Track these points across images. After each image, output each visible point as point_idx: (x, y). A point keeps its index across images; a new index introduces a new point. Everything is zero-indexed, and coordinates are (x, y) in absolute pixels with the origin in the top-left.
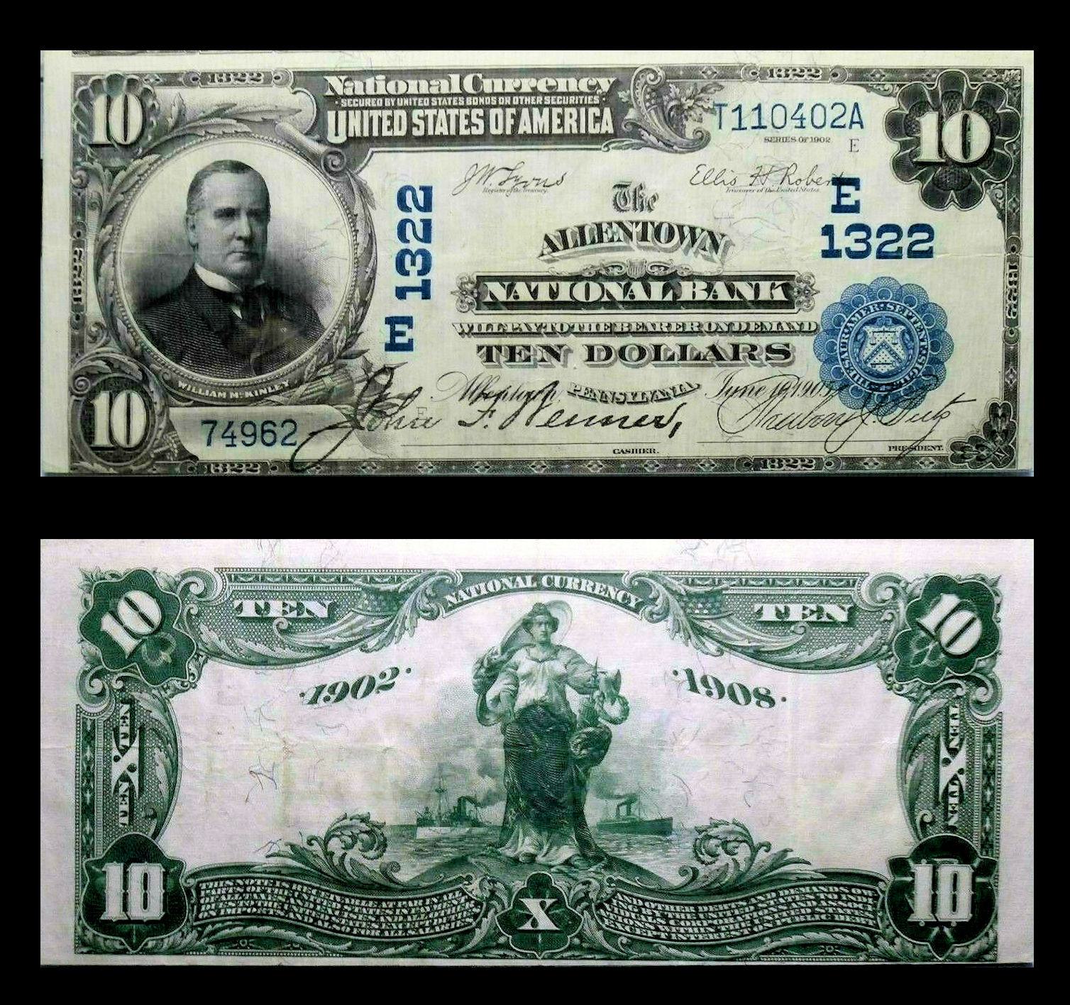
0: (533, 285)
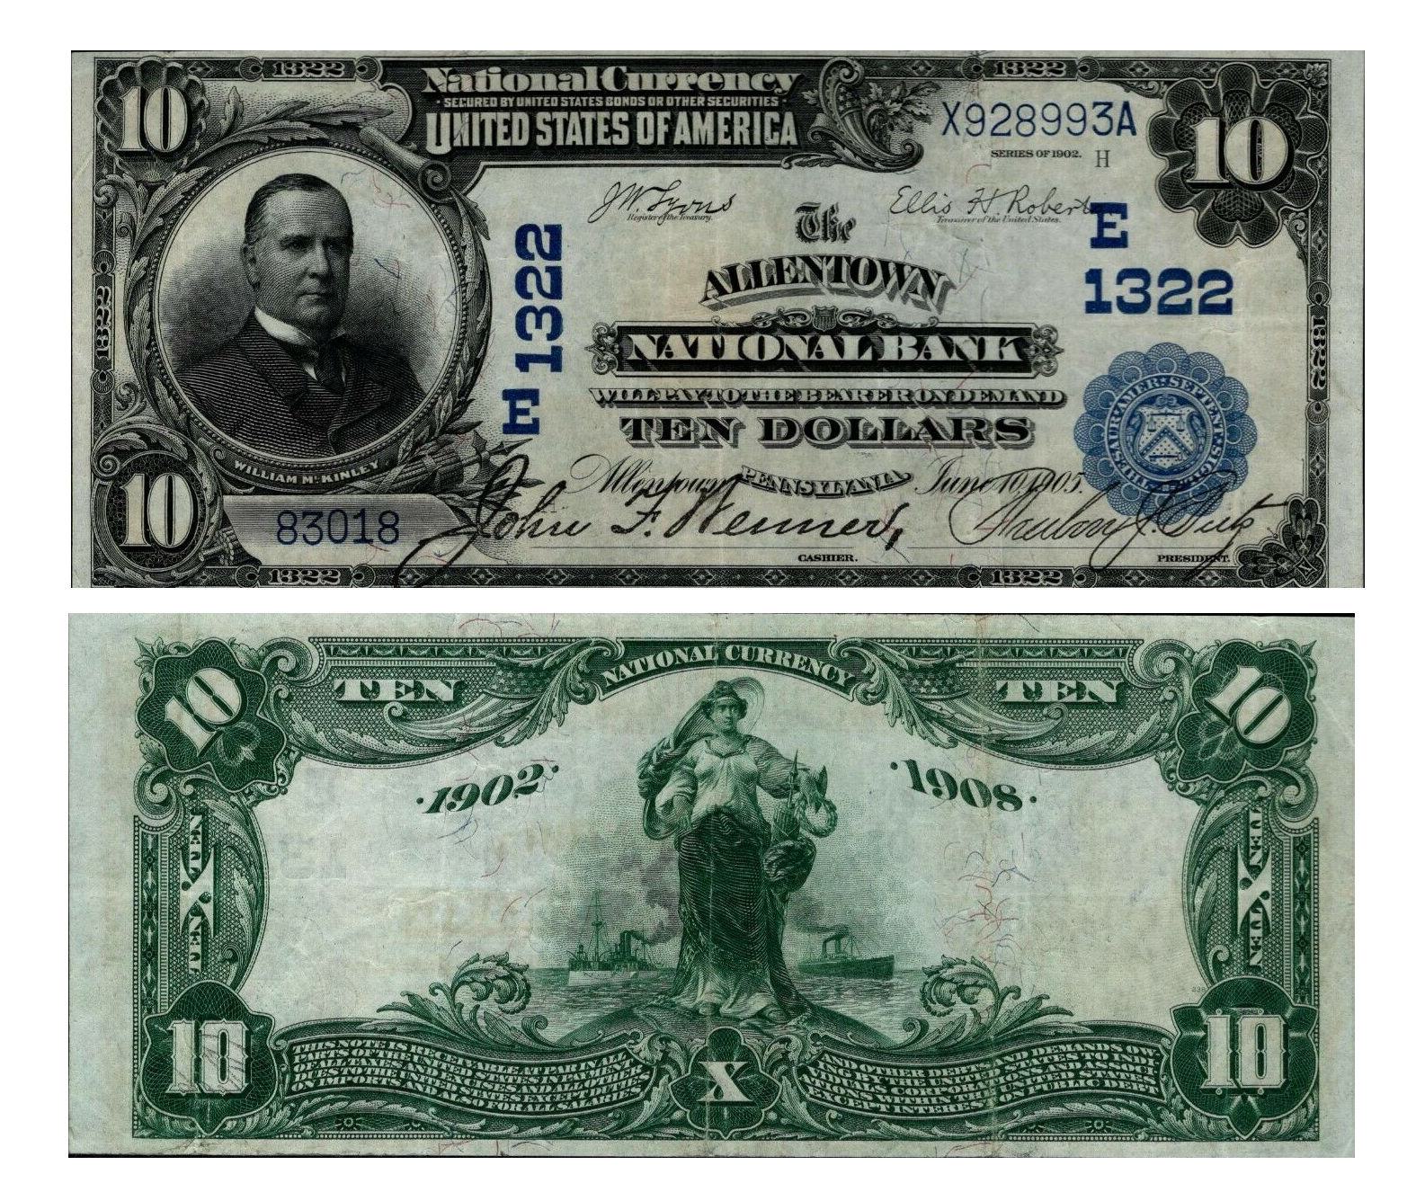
0: (692, 339)
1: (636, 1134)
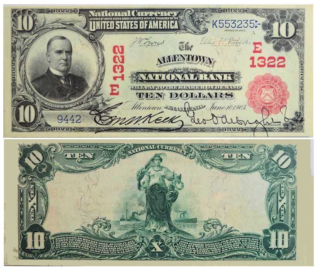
1: (136, 259)
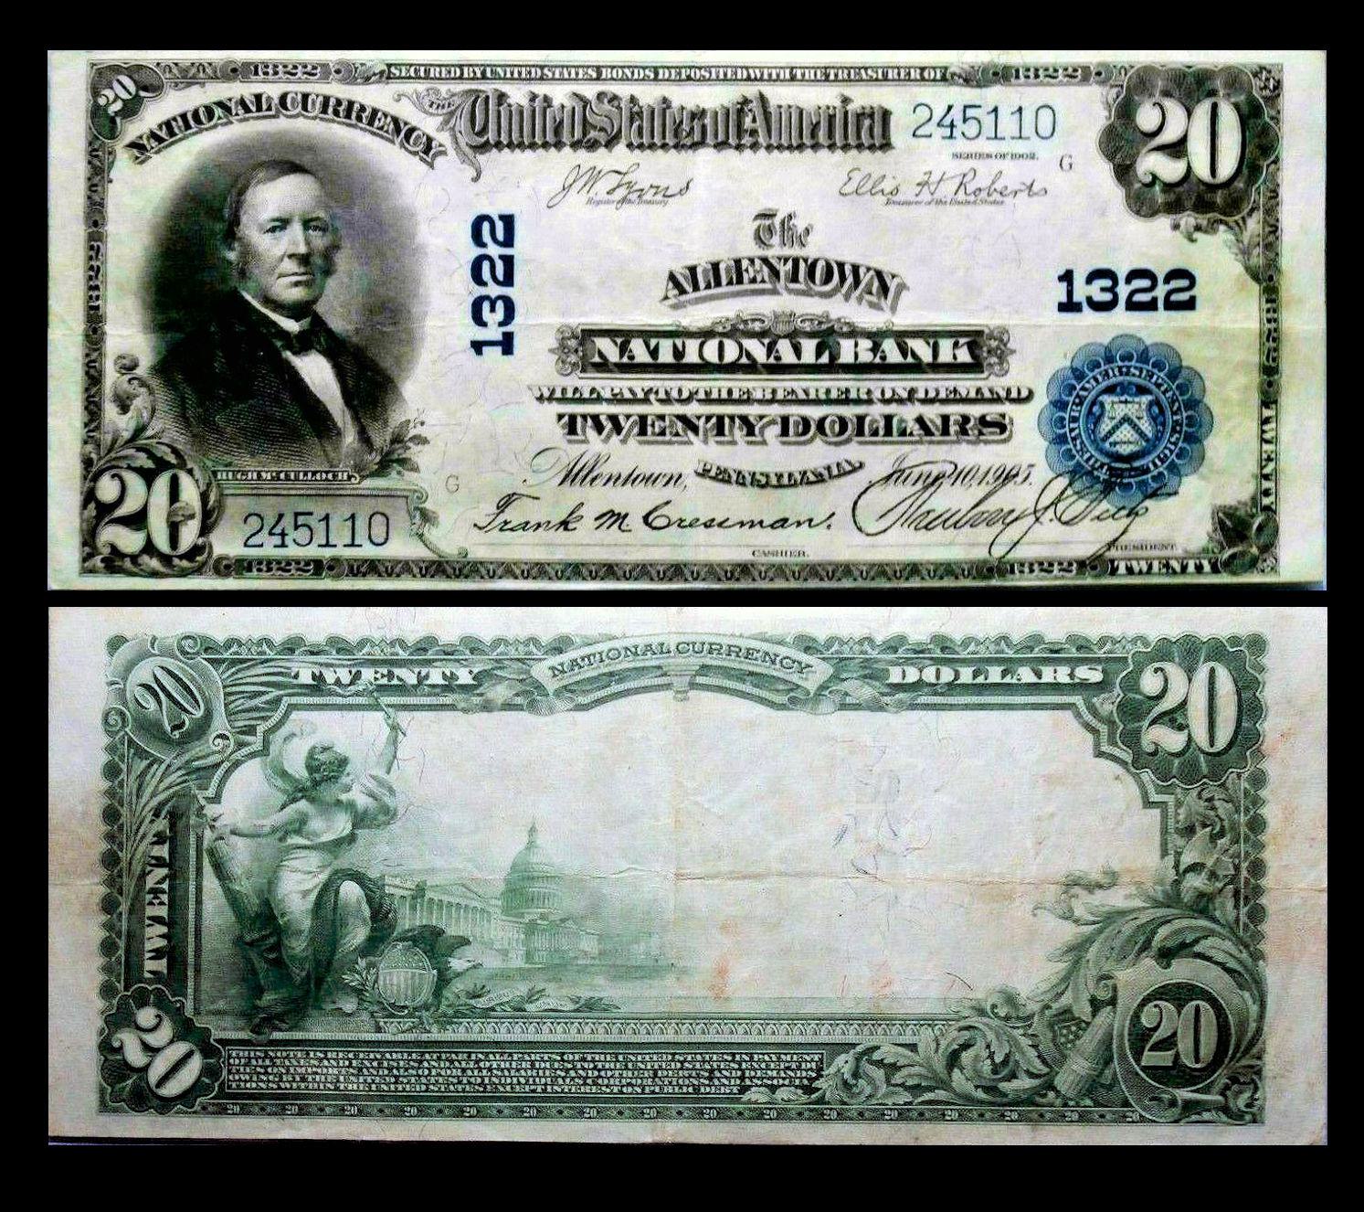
0: (653, 342)
